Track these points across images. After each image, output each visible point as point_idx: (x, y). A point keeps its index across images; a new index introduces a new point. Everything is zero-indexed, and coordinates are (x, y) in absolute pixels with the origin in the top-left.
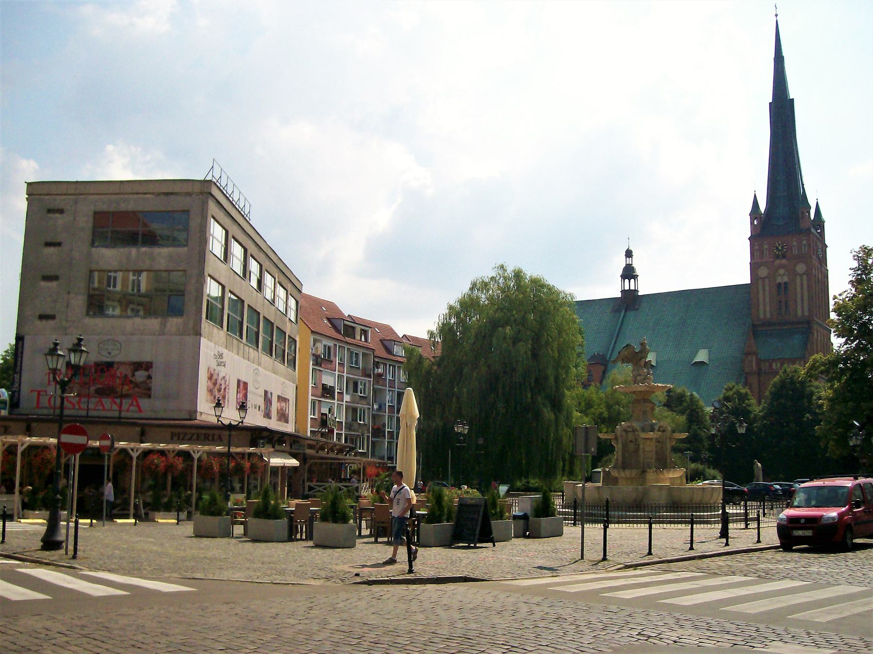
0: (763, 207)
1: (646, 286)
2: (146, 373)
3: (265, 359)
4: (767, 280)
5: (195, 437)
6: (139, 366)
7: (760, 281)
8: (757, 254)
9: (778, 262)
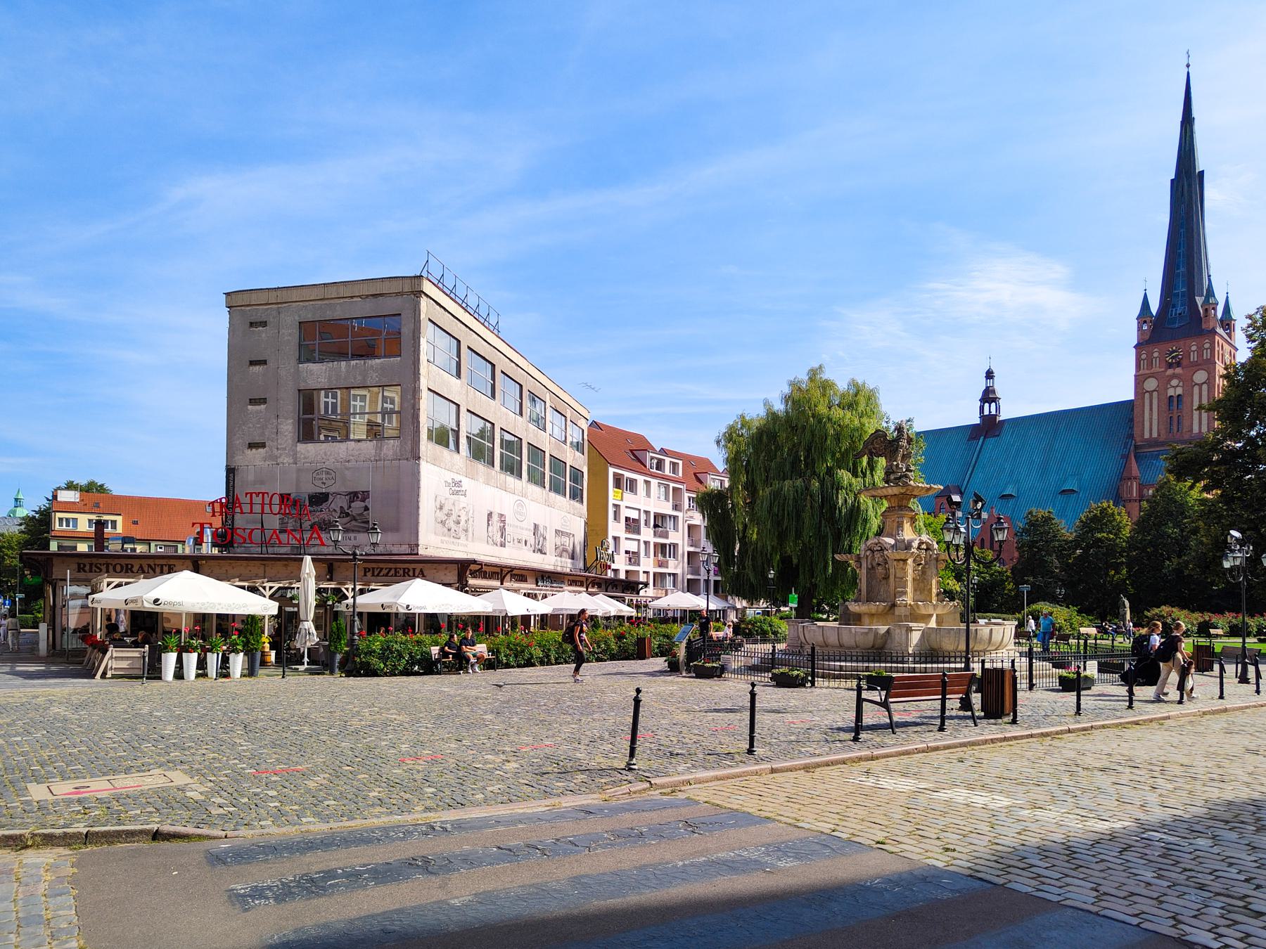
0: (1154, 307)
1: (1009, 410)
2: (363, 504)
3: (534, 490)
4: (1155, 394)
5: (392, 572)
6: (353, 496)
7: (1147, 395)
8: (1144, 364)
9: (1170, 372)
